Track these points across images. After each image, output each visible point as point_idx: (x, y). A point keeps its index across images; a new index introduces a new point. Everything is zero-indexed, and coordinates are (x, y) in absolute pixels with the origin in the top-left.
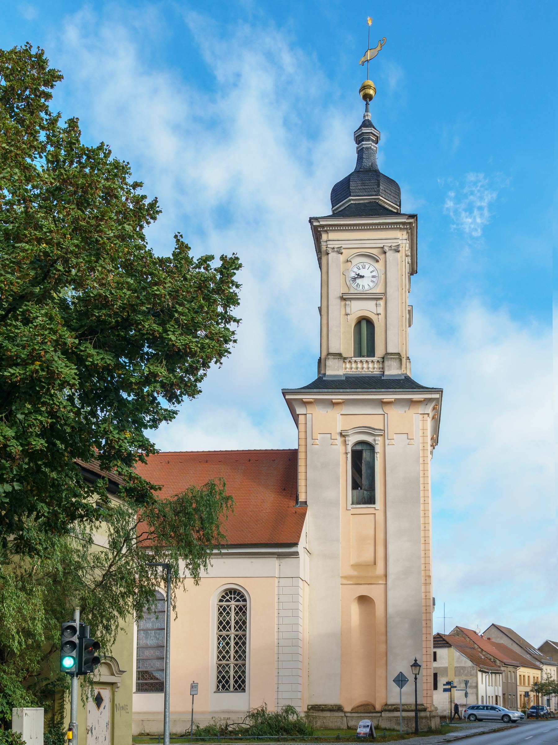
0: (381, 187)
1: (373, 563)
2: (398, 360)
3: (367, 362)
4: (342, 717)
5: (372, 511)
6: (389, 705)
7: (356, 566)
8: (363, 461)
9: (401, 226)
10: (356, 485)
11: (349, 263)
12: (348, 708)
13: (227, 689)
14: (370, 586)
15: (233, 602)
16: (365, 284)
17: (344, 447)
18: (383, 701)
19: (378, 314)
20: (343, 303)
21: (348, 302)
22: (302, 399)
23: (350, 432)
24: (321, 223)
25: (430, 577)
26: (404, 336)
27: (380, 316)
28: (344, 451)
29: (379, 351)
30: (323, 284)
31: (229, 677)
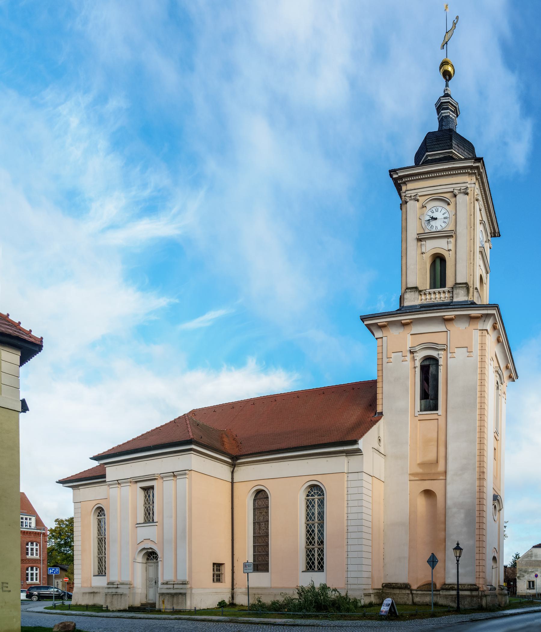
0: (453, 141)
1: (436, 462)
2: (465, 289)
3: (439, 293)
4: (408, 594)
5: (435, 417)
6: (447, 584)
7: (422, 465)
8: (430, 375)
9: (469, 171)
10: (424, 395)
11: (425, 208)
12: (414, 587)
13: (313, 569)
14: (432, 481)
15: (316, 497)
16: (438, 225)
17: (413, 363)
18: (442, 581)
19: (449, 250)
20: (419, 243)
21: (423, 243)
22: (376, 324)
23: (417, 348)
24: (399, 174)
25: (484, 472)
26: (472, 268)
27: (450, 252)
28: (413, 366)
29: (450, 282)
30: (403, 230)
31: (314, 559)
